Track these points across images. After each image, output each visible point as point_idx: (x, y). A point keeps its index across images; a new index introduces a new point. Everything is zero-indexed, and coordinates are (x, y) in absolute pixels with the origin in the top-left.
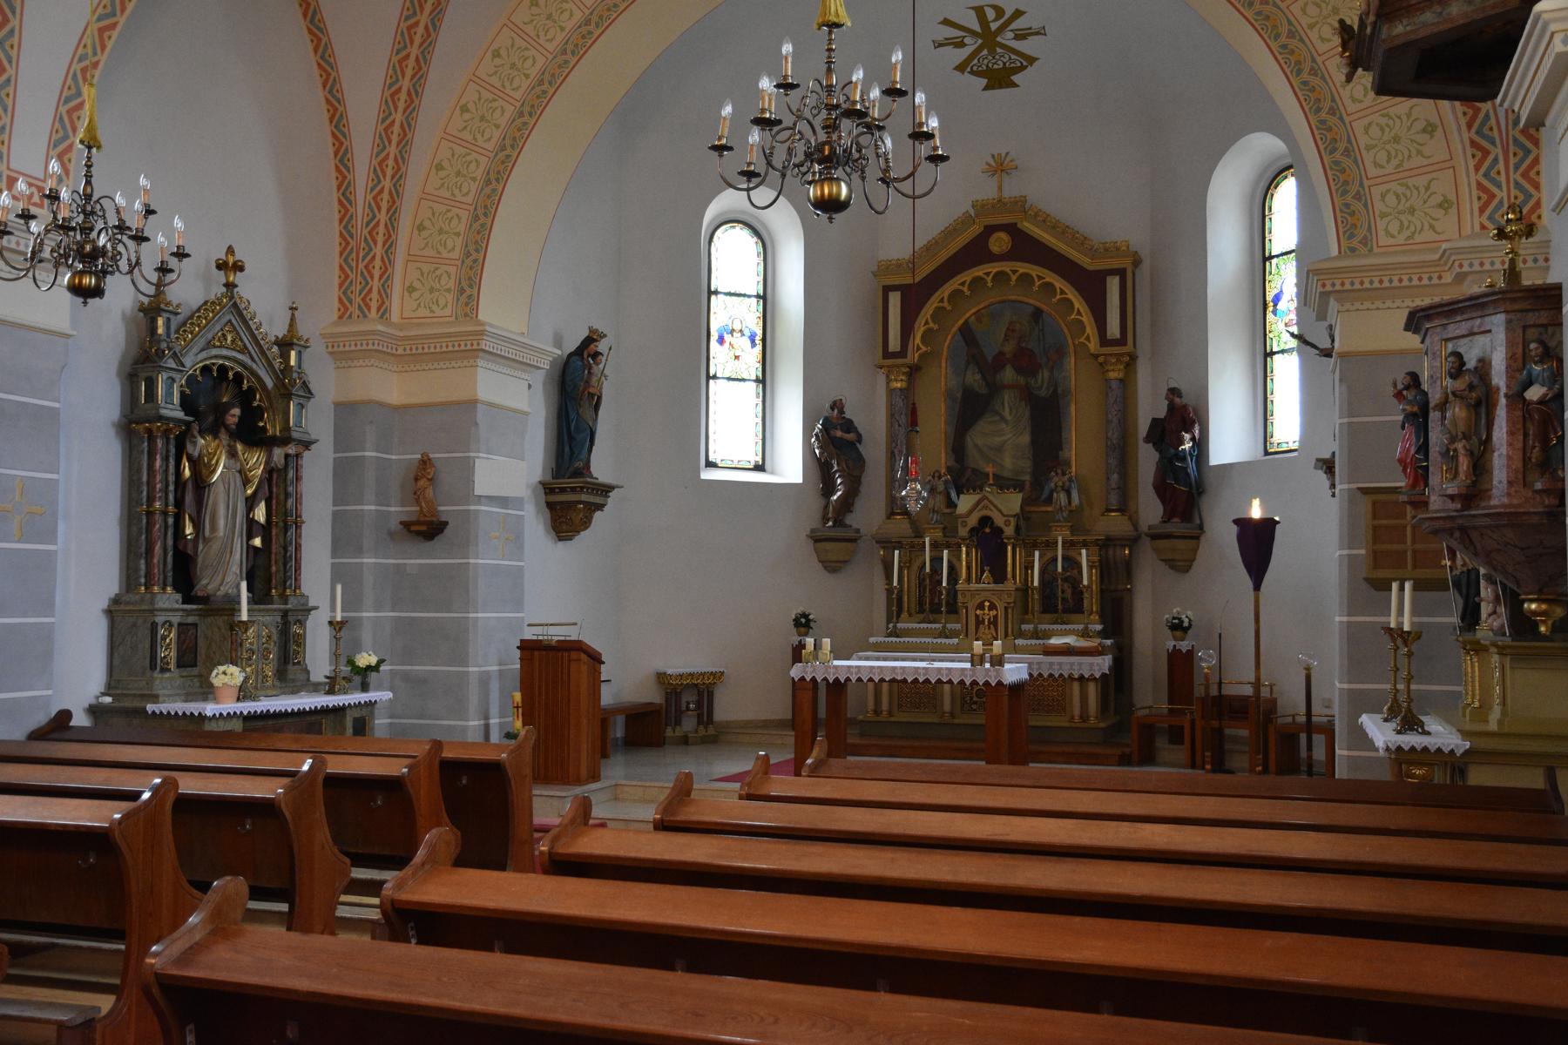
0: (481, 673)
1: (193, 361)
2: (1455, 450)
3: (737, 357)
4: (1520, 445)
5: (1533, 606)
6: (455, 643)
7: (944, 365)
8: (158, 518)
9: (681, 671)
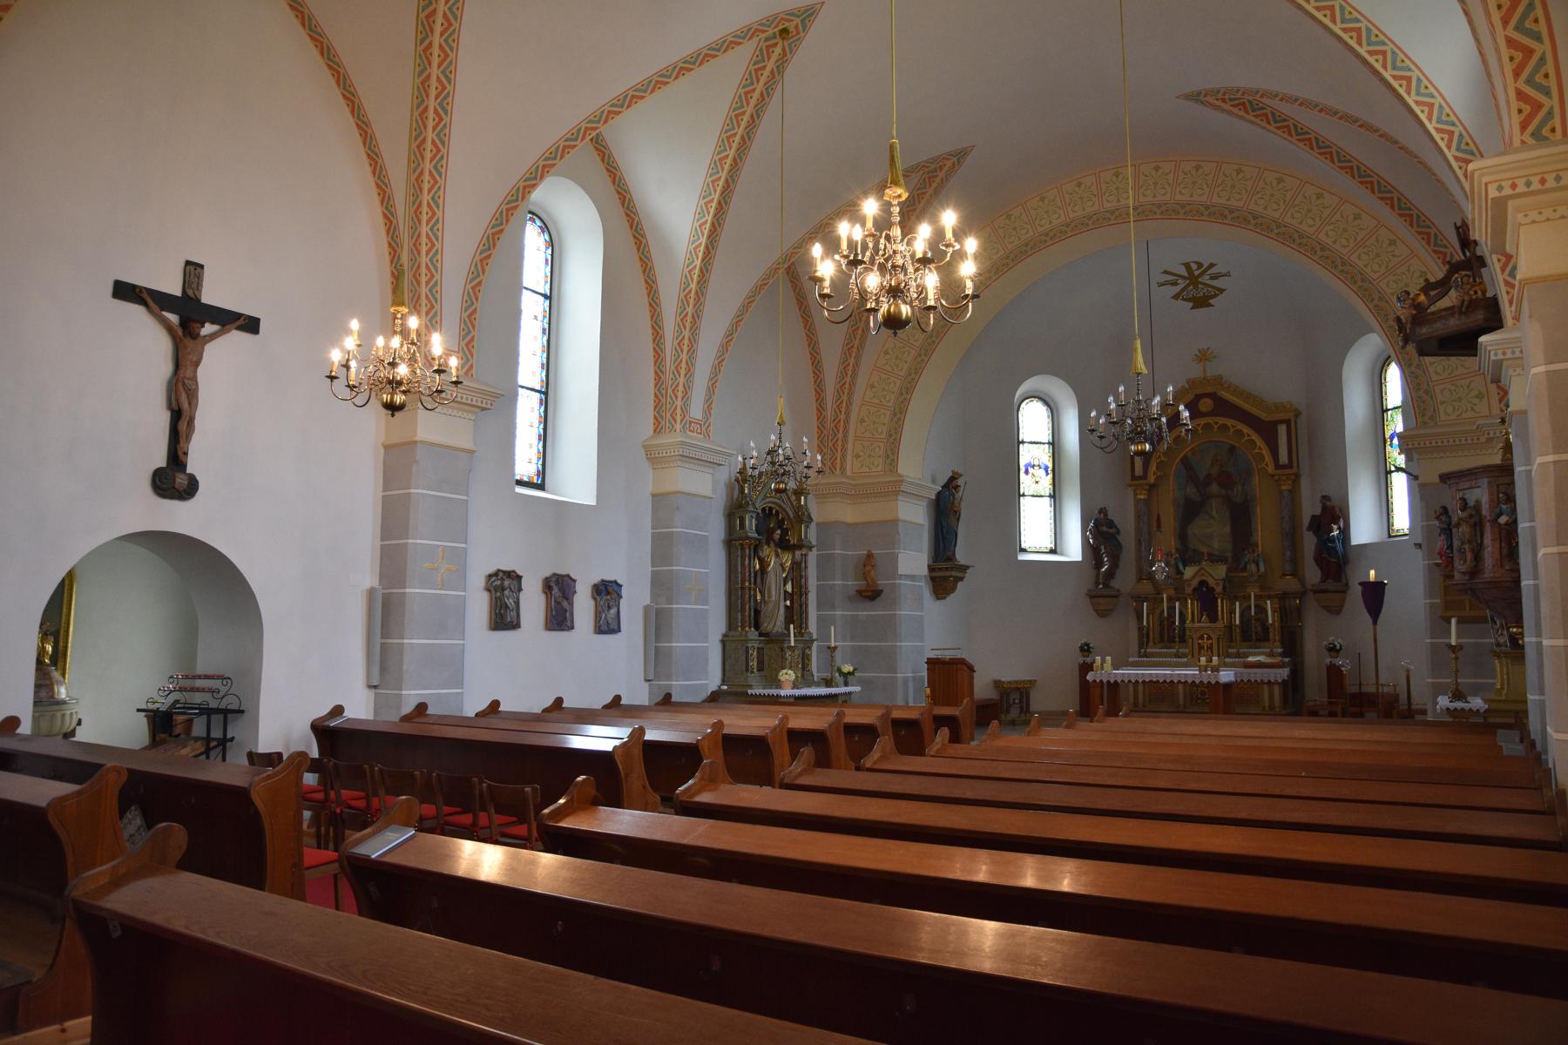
0: (904, 677)
1: (759, 505)
2: (1464, 549)
3: (1037, 482)
4: (1498, 546)
5: (1515, 630)
6: (889, 660)
7: (1171, 482)
8: (747, 591)
9: (1009, 679)
